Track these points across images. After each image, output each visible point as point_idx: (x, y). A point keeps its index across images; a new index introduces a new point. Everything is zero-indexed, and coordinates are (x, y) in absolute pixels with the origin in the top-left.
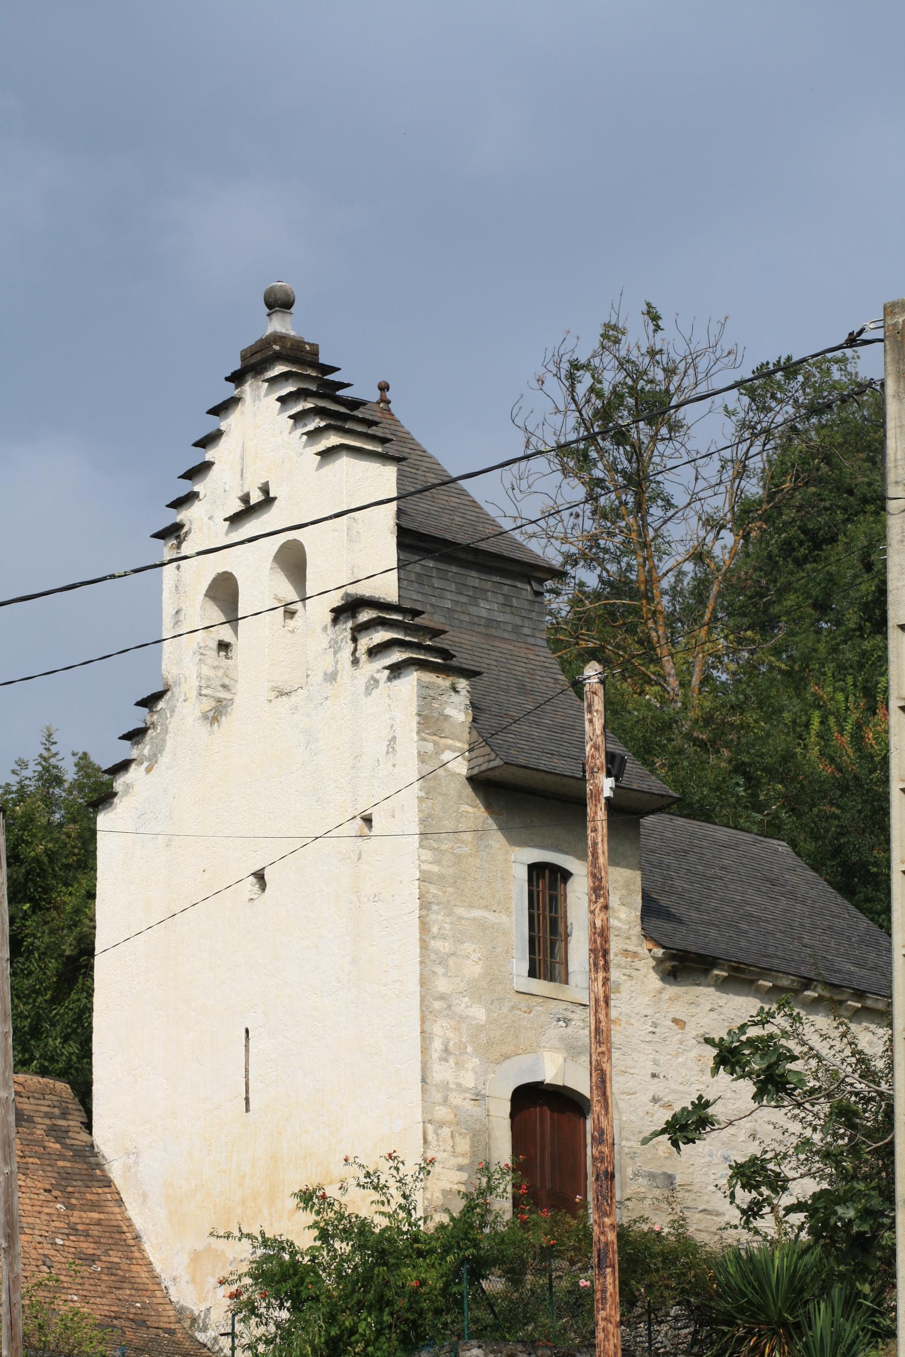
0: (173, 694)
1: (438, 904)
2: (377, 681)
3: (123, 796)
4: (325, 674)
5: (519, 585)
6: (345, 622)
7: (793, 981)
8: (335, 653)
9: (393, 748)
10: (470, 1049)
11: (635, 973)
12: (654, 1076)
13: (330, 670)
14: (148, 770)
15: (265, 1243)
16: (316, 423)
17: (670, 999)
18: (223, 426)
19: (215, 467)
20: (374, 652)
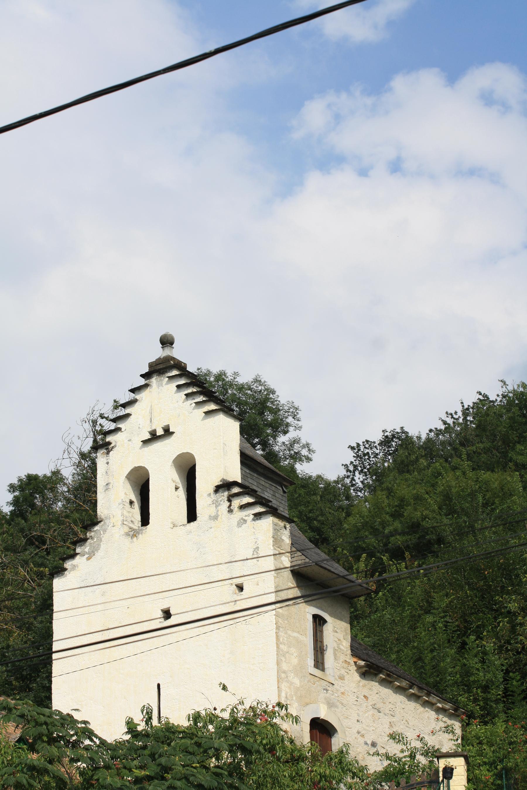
0: (105, 523)
1: (282, 628)
2: (245, 521)
3: (71, 571)
4: (210, 516)
5: (278, 487)
6: (223, 492)
7: (407, 684)
8: (216, 507)
9: (257, 553)
10: (294, 698)
11: (349, 672)
12: (358, 721)
13: (213, 514)
14: (88, 559)
15: (388, 758)
16: (201, 398)
17: (363, 686)
18: (138, 397)
19: (131, 417)
20: (242, 507)
